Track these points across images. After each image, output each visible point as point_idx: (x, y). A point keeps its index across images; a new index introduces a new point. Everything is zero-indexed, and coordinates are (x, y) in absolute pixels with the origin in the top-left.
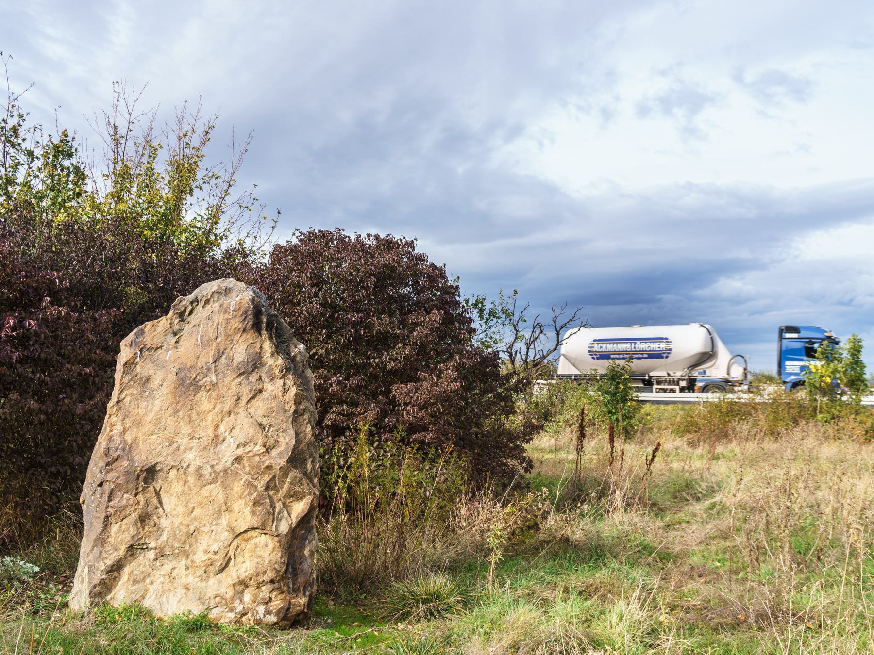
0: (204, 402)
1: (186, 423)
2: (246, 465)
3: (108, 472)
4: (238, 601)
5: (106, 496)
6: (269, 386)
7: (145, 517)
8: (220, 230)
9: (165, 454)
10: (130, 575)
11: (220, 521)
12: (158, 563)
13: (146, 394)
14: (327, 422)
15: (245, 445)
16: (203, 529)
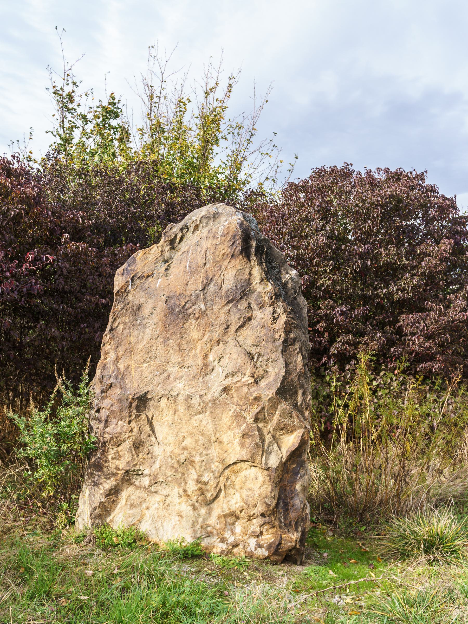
0: (194, 330)
2: (235, 395)
4: (229, 532)
7: (139, 444)
8: (241, 176)
9: (155, 383)
10: (127, 499)
13: (138, 322)
15: (233, 374)
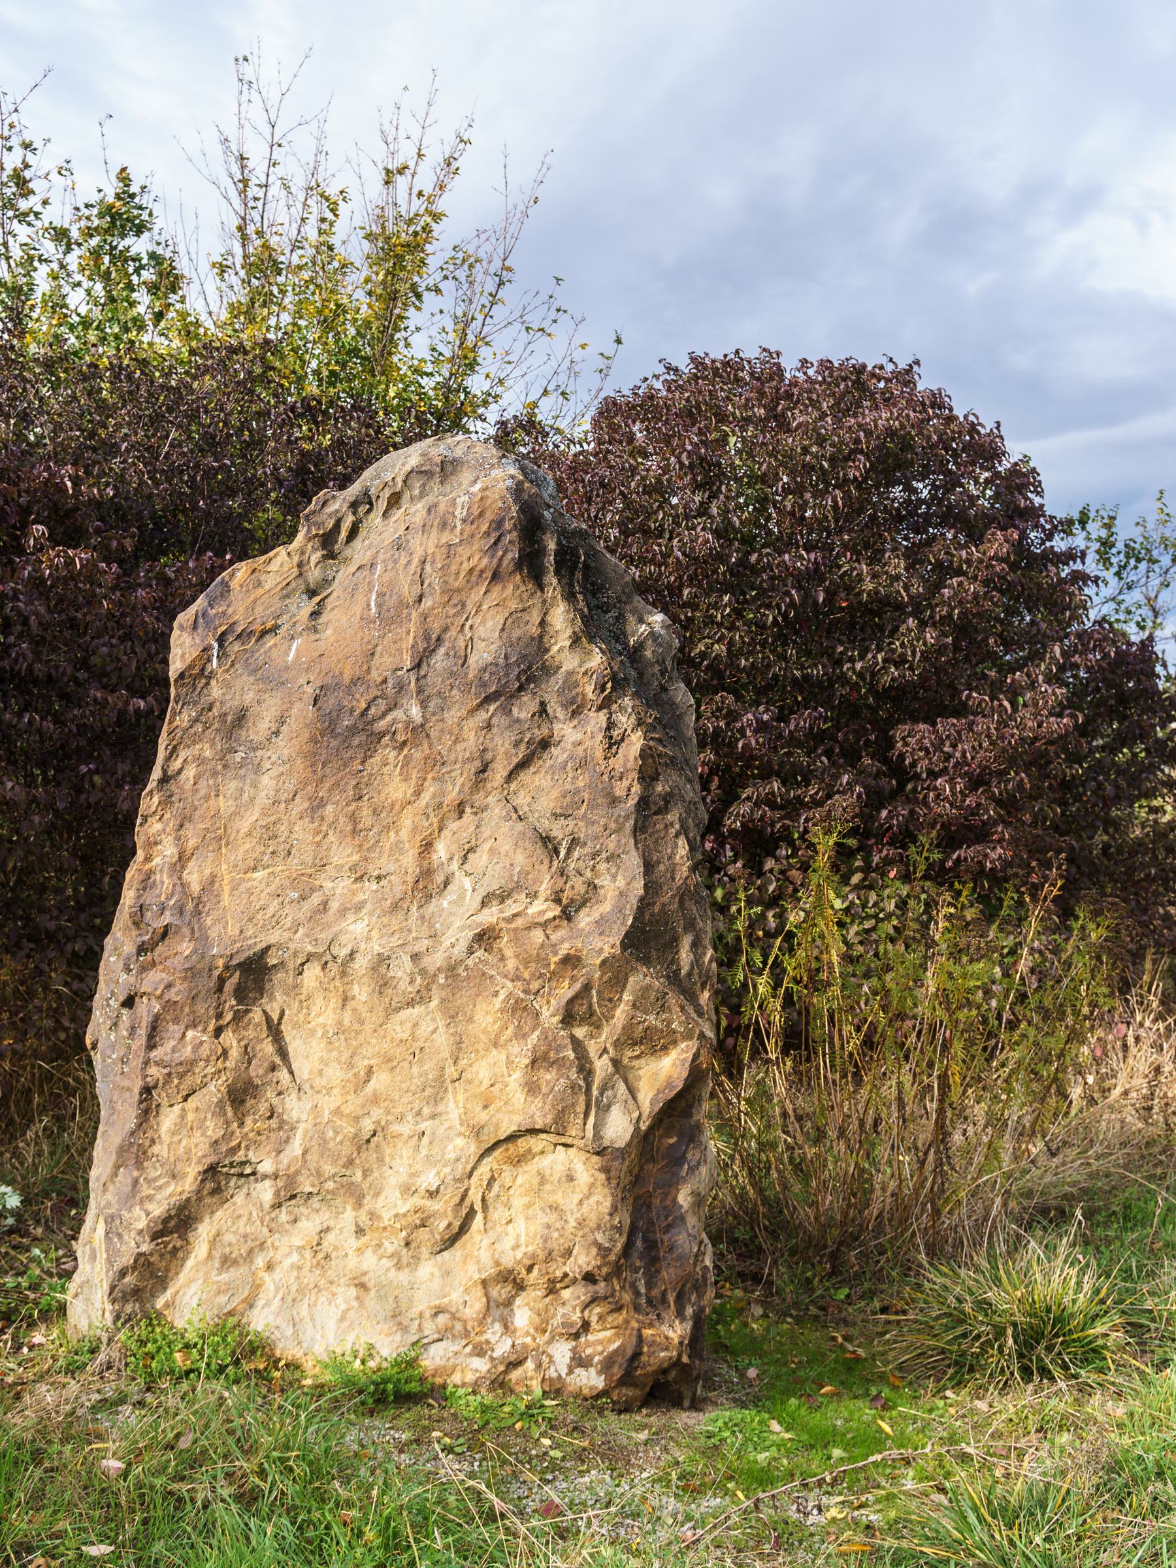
1: (342, 835)
2: (508, 953)
3: (144, 969)
4: (498, 1327)
5: (142, 1032)
6: (567, 732)
7: (245, 1091)
9: (288, 922)
10: (213, 1243)
11: (441, 1108)
12: (283, 1216)
13: (238, 757)
14: (732, 823)
16: (396, 1128)
